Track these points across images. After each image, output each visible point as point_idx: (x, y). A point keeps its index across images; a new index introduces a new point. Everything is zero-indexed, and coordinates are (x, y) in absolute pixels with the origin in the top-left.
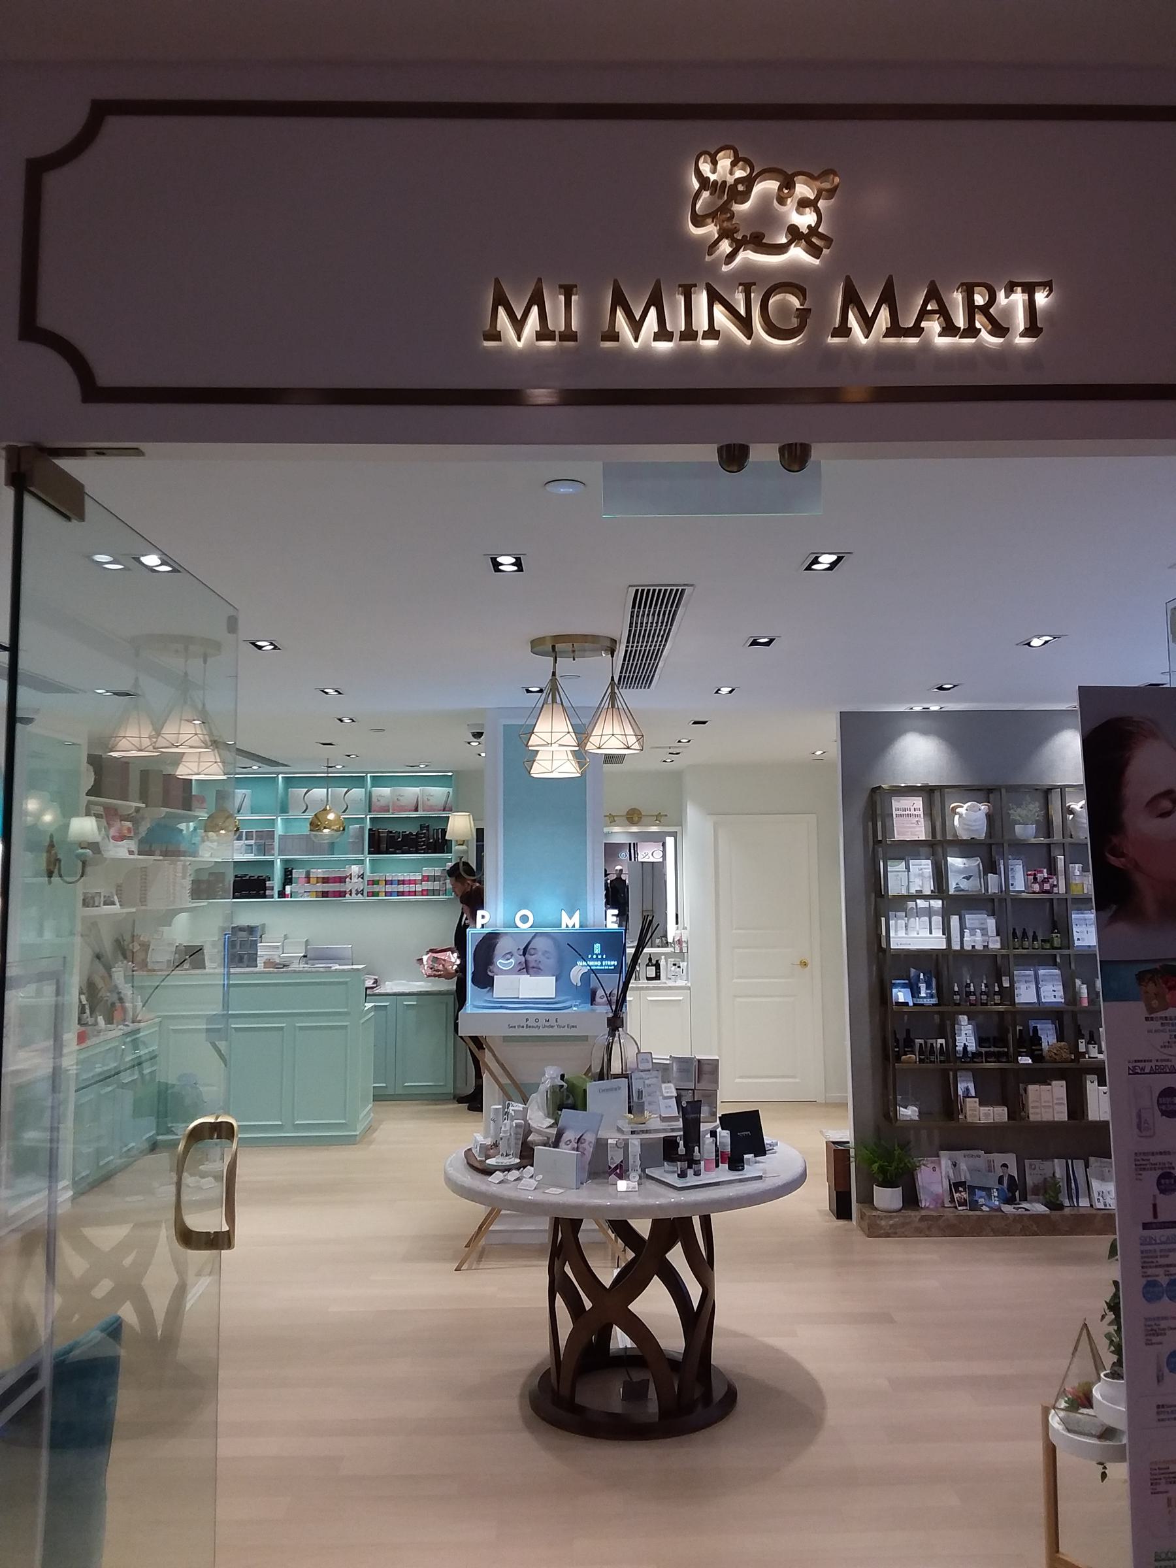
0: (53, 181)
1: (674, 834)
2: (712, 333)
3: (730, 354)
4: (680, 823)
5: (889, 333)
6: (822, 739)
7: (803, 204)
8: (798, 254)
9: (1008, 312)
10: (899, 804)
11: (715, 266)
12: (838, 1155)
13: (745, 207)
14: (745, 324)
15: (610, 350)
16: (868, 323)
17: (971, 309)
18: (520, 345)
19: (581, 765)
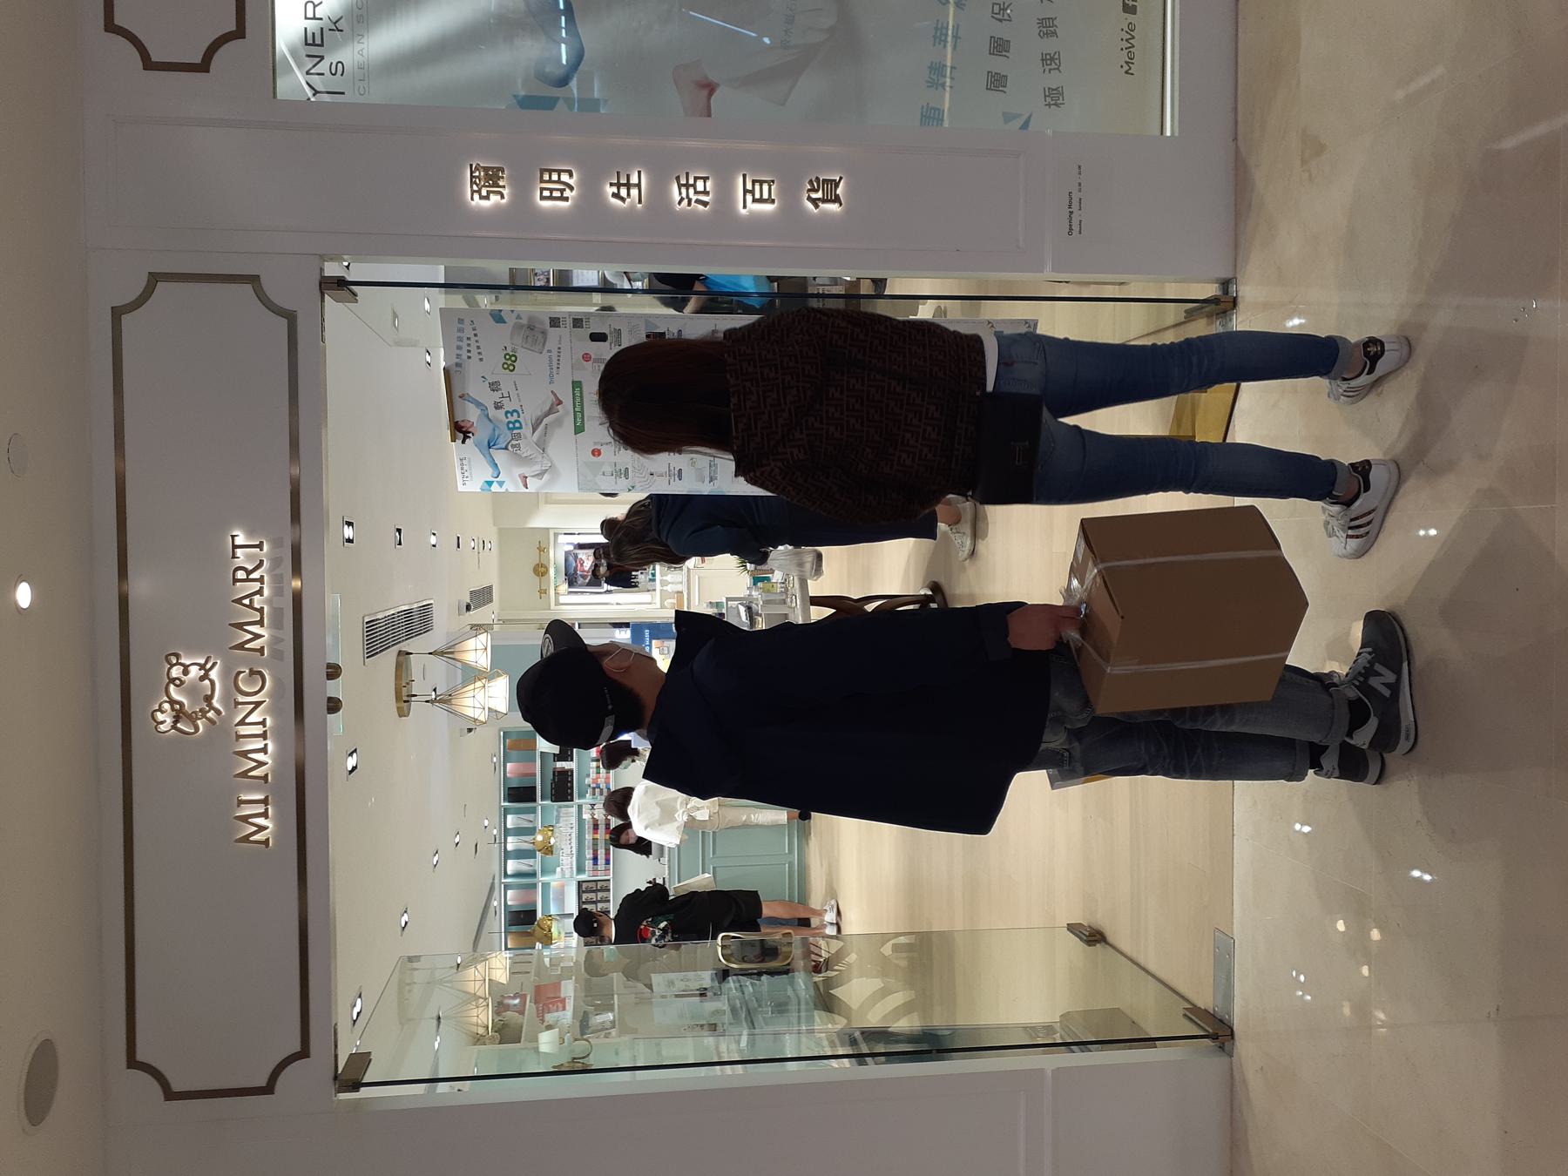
0: (177, 1087)
1: (556, 535)
2: (263, 723)
3: (274, 710)
7: (186, 672)
8: (213, 674)
14: (258, 704)
16: (257, 636)
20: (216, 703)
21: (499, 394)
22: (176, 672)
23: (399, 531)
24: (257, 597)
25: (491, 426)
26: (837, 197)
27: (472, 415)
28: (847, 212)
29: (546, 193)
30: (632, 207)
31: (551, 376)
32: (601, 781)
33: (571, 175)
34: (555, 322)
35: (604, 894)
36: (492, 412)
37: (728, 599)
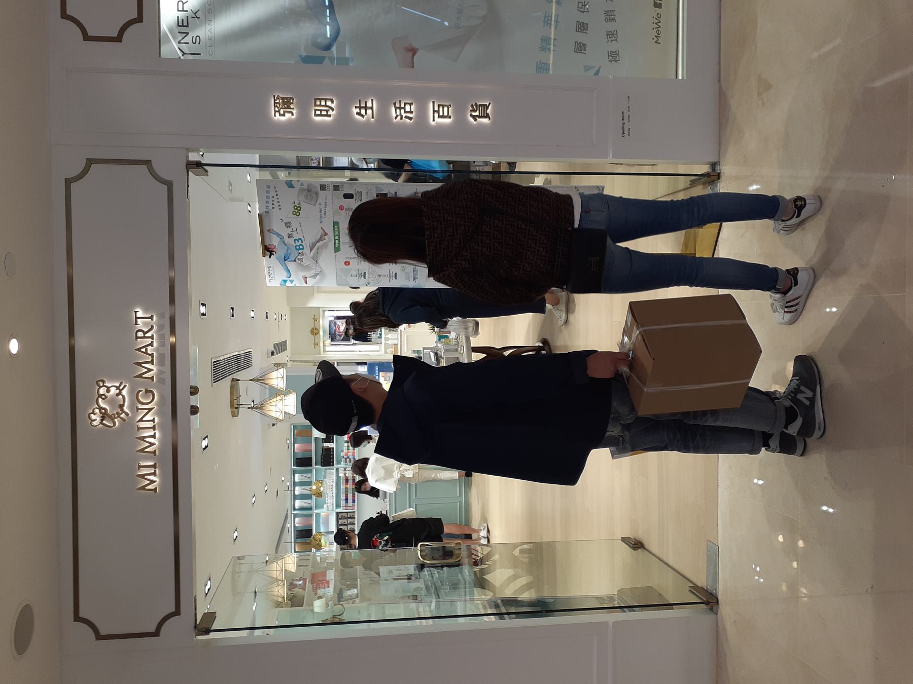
0: (103, 632)
1: (324, 311)
2: (153, 421)
3: (160, 413)
7: (108, 391)
8: (124, 392)
14: (150, 410)
16: (150, 370)
20: (125, 409)
21: (290, 229)
22: (102, 391)
23: (232, 309)
24: (149, 347)
25: (286, 248)
26: (488, 115)
27: (275, 241)
28: (493, 123)
29: (318, 112)
30: (368, 120)
31: (321, 219)
32: (350, 454)
33: (332, 102)
34: (323, 187)
35: (352, 520)
36: (286, 240)
37: (424, 349)
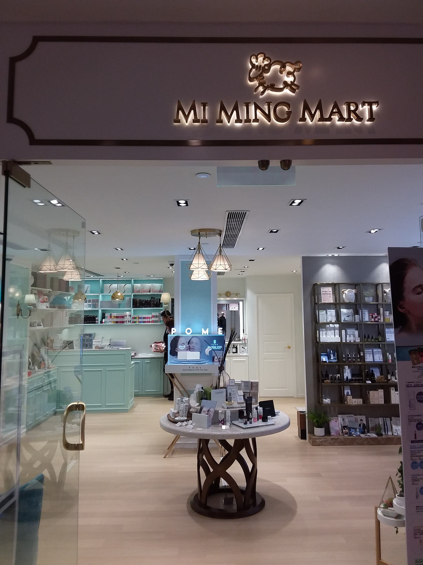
0: (19, 65)
1: (242, 301)
2: (256, 120)
3: (262, 128)
4: (245, 296)
5: (320, 120)
6: (296, 266)
7: (289, 73)
8: (287, 91)
9: (363, 112)
10: (323, 290)
11: (257, 96)
12: (302, 416)
13: (268, 74)
14: (268, 117)
15: (219, 126)
16: (312, 116)
17: (349, 111)
18: (187, 124)
19: (209, 276)
